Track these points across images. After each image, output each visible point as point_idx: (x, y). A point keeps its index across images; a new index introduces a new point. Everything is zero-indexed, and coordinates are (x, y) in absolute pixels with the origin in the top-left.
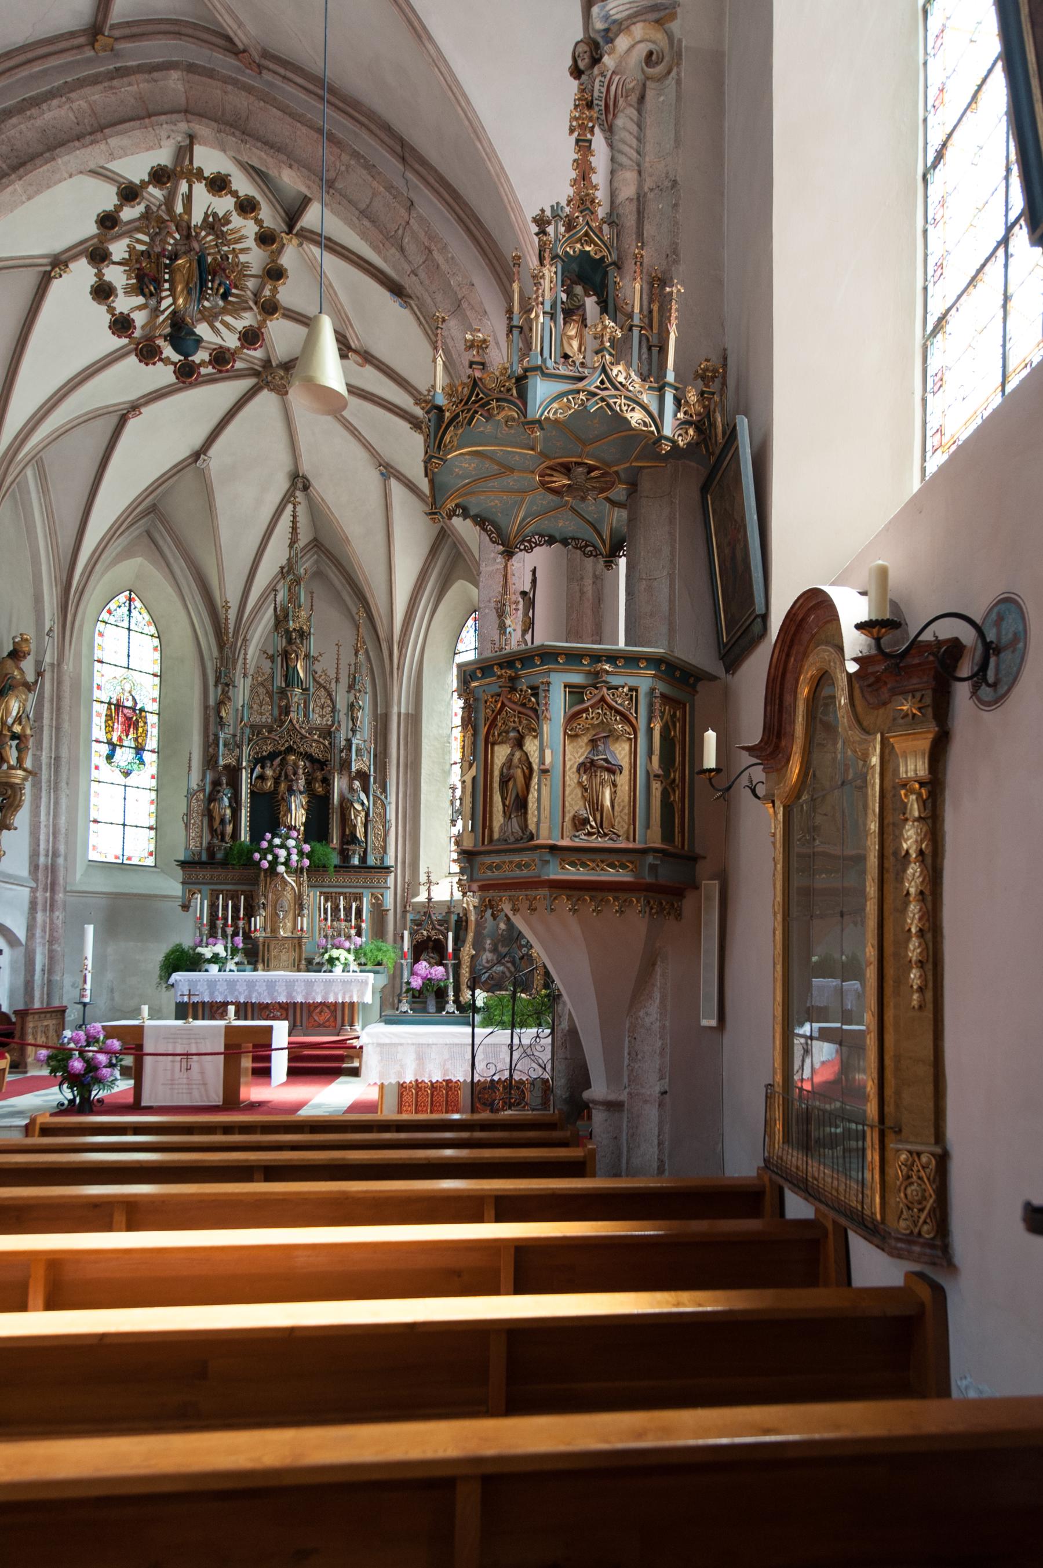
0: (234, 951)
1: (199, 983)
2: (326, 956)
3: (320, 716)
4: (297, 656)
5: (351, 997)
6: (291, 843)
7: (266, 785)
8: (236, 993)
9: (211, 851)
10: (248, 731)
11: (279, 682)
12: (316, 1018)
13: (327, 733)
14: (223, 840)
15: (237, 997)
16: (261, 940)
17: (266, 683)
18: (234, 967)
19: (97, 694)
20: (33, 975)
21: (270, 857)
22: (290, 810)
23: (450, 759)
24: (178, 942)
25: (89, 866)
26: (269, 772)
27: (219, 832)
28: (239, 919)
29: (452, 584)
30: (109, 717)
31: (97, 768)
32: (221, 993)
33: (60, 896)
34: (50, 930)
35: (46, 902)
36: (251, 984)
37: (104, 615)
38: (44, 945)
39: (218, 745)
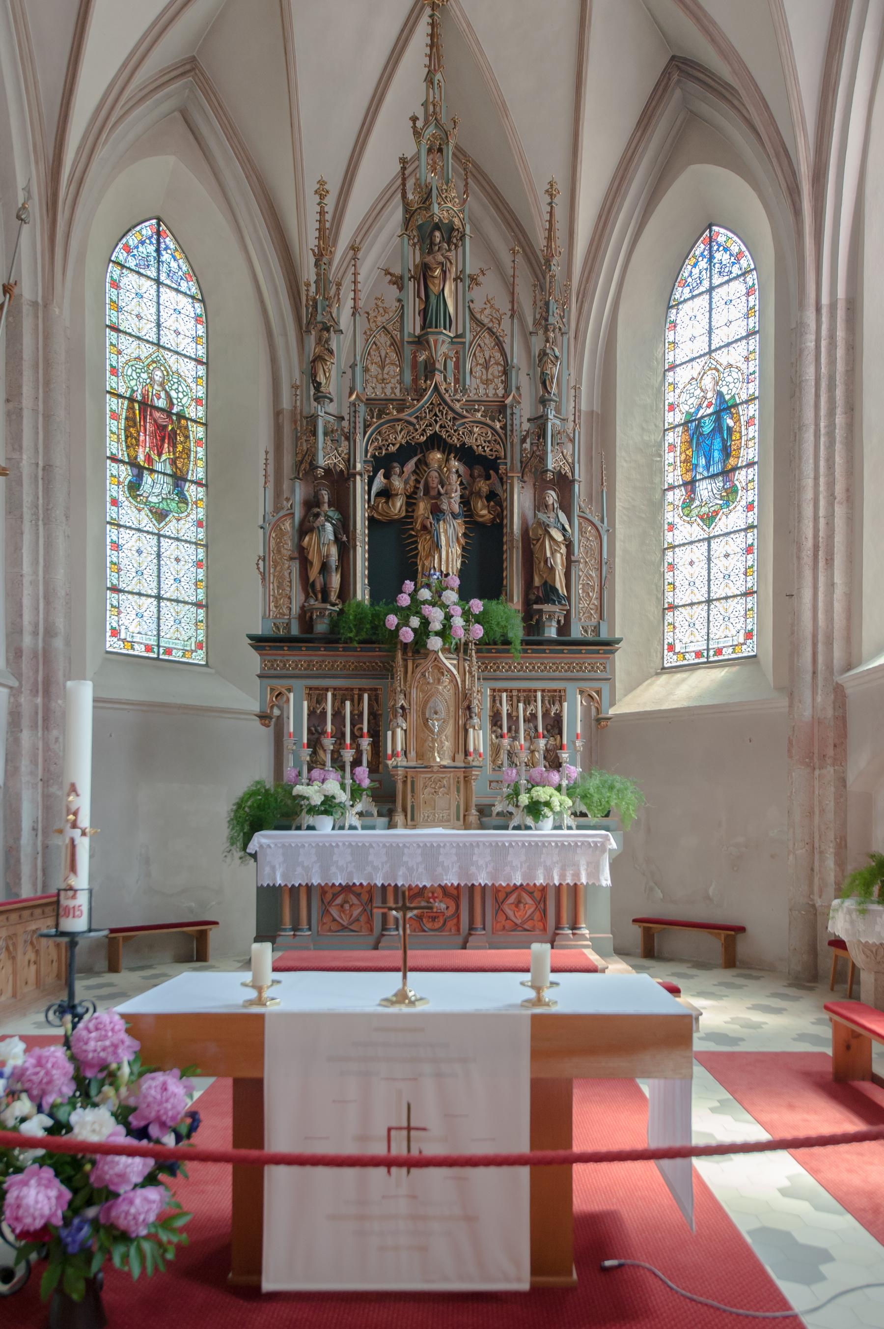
0: (356, 793)
1: (301, 851)
2: (524, 799)
4: (444, 272)
5: (577, 875)
6: (451, 596)
7: (394, 505)
8: (369, 869)
9: (306, 620)
10: (362, 409)
11: (413, 325)
12: (510, 913)
13: (501, 409)
14: (325, 599)
16: (400, 772)
17: (390, 327)
18: (355, 821)
20: (18, 839)
22: (437, 547)
23: (662, 482)
24: (257, 778)
26: (398, 483)
27: (318, 587)
28: (537, 736)
30: (130, 421)
31: (115, 502)
34: (45, 760)
35: (37, 713)
36: (394, 852)
37: (120, 254)
38: (35, 786)
39: (314, 433)
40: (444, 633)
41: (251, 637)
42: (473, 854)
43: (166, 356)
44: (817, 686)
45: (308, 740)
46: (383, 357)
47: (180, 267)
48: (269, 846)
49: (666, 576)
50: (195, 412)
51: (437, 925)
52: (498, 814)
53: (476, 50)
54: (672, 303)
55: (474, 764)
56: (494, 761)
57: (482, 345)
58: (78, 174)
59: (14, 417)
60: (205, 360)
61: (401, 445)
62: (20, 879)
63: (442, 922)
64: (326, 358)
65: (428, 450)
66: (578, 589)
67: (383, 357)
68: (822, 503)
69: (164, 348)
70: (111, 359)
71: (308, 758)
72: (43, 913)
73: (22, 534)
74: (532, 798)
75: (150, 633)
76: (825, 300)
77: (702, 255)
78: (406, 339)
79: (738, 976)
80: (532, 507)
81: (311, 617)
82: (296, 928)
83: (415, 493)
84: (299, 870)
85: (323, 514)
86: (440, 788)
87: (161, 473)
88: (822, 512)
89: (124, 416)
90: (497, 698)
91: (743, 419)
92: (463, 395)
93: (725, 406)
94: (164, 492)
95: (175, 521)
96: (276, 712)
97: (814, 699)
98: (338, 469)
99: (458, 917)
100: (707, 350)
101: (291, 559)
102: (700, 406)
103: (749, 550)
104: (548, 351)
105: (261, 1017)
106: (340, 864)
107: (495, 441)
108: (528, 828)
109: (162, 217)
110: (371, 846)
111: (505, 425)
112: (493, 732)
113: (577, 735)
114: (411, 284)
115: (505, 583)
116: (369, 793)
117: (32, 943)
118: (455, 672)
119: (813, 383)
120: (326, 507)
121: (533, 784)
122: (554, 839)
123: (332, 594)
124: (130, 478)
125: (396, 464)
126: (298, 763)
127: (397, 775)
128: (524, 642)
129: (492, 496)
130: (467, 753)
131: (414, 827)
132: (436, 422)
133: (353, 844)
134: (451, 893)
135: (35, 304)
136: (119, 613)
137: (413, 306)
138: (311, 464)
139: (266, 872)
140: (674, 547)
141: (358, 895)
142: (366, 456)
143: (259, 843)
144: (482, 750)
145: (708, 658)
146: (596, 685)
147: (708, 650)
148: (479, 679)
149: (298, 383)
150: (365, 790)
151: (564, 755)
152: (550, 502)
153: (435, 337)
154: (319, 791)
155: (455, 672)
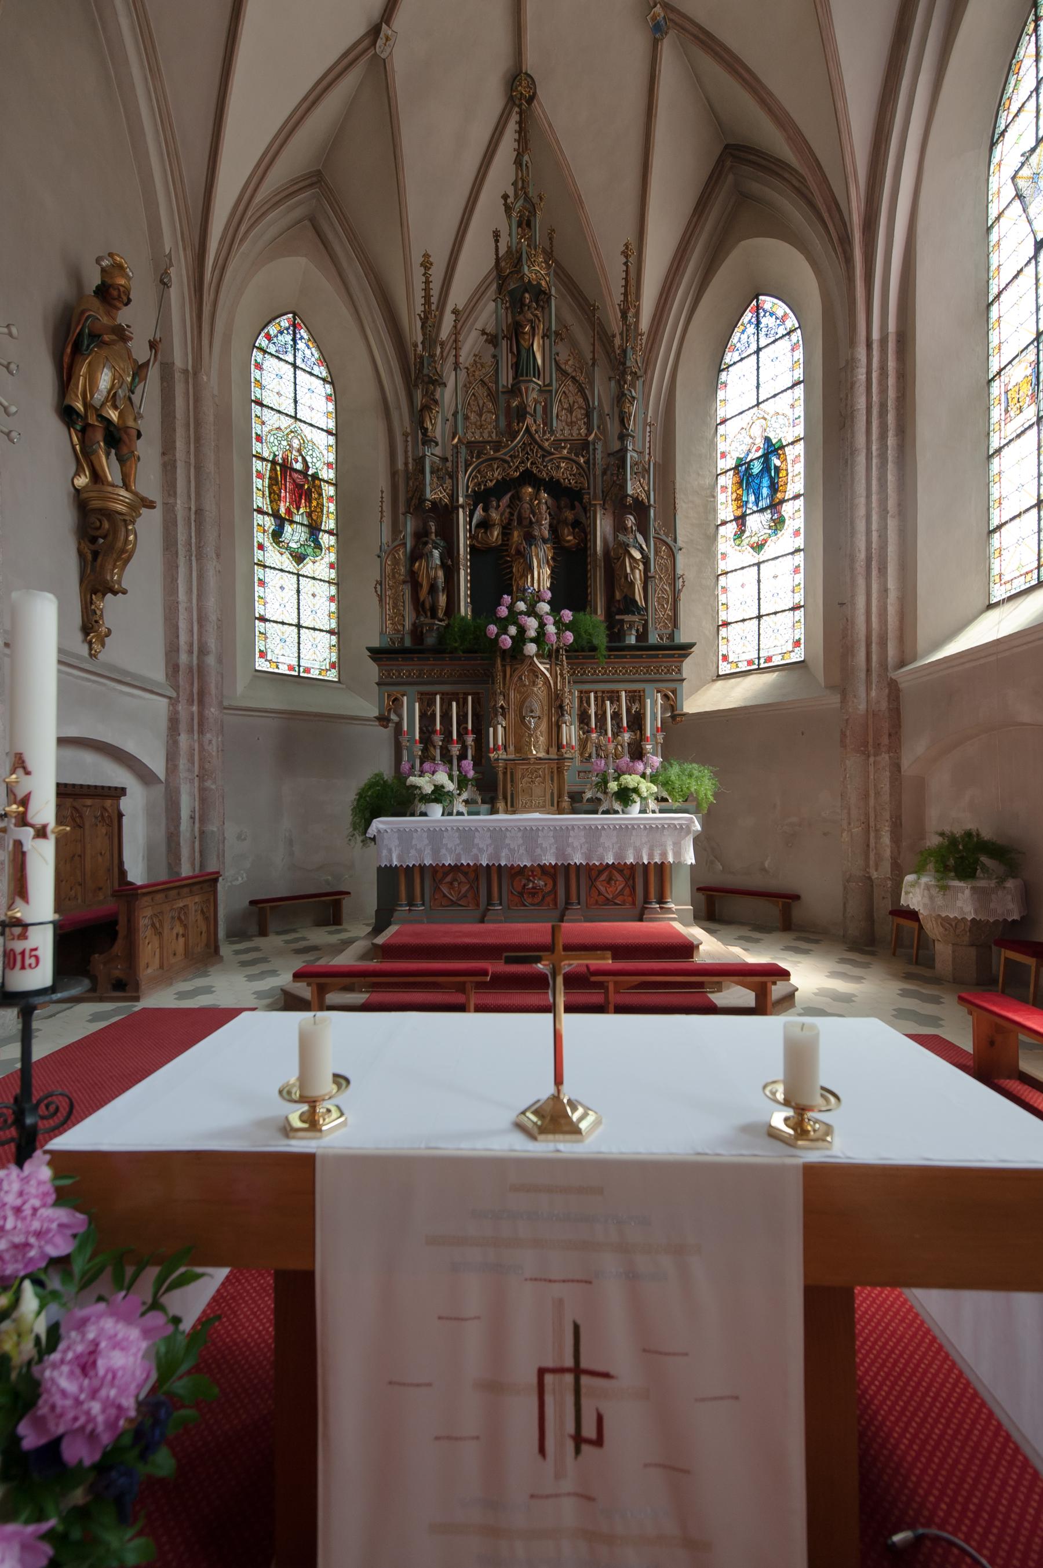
0: (462, 783)
1: (415, 835)
2: (613, 786)
3: (567, 424)
4: (533, 328)
5: (664, 854)
6: (544, 607)
7: (492, 535)
8: (475, 851)
9: (417, 633)
10: (463, 450)
11: (506, 378)
12: (602, 889)
14: (434, 615)
15: (476, 857)
17: (486, 379)
18: (462, 808)
19: (257, 447)
20: (178, 825)
21: (513, 630)
22: (531, 570)
23: (715, 518)
24: (376, 772)
25: (255, 676)
26: (495, 515)
27: (427, 606)
29: (728, 254)
30: (273, 480)
32: (450, 851)
33: (212, 711)
34: (200, 759)
35: (193, 719)
36: (498, 835)
37: (262, 341)
38: (192, 781)
40: (540, 638)
41: (369, 649)
42: (568, 837)
43: (302, 428)
44: (871, 683)
45: (420, 737)
46: (481, 405)
47: (313, 355)
48: (386, 831)
49: (720, 598)
50: (327, 474)
51: (536, 900)
52: (588, 800)
53: (556, 147)
54: (723, 367)
55: (567, 756)
56: (581, 754)
57: (567, 392)
58: (220, 262)
59: (169, 468)
60: (334, 432)
61: (498, 481)
62: (180, 860)
63: (541, 897)
64: (432, 407)
65: (520, 485)
66: (652, 603)
67: (481, 405)
68: (875, 518)
69: (300, 421)
70: (256, 428)
71: (420, 753)
72: (191, 891)
73: (177, 567)
74: (621, 785)
75: (291, 655)
76: (876, 335)
77: (750, 322)
78: (500, 389)
79: (798, 939)
80: (612, 532)
81: (422, 632)
82: (411, 903)
83: (509, 524)
84: (413, 852)
85: (431, 541)
86: (536, 778)
87: (299, 523)
88: (874, 526)
89: (268, 476)
90: (584, 699)
91: (790, 458)
92: (551, 436)
93: (773, 448)
94: (302, 539)
95: (311, 563)
96: (393, 717)
97: (868, 694)
98: (443, 503)
99: (556, 892)
100: (755, 403)
101: (404, 582)
102: (749, 451)
103: (796, 570)
104: (626, 392)
105: (308, 1160)
106: (449, 846)
107: (580, 474)
108: (616, 812)
109: (297, 312)
110: (477, 830)
111: (588, 460)
112: (581, 728)
113: (657, 728)
114: (504, 342)
115: (589, 598)
116: (474, 783)
117: (179, 918)
118: (548, 675)
119: (865, 412)
120: (433, 536)
121: (619, 773)
122: (643, 822)
123: (440, 611)
124: (273, 527)
125: (493, 499)
126: (411, 758)
127: (498, 767)
128: (610, 649)
129: (576, 524)
130: (560, 746)
131: (514, 812)
132: (528, 459)
133: (461, 828)
134: (549, 872)
135: (185, 372)
136: (266, 638)
137: (506, 360)
138: (420, 498)
139: (384, 854)
140: (727, 573)
141: (465, 874)
142: (467, 491)
143: (377, 828)
144: (574, 743)
145: (759, 665)
146: (672, 685)
147: (759, 658)
148: (569, 682)
149: (409, 430)
150: (470, 780)
151: (648, 747)
152: (629, 525)
153: (527, 385)
154: (430, 782)
155: (548, 675)
